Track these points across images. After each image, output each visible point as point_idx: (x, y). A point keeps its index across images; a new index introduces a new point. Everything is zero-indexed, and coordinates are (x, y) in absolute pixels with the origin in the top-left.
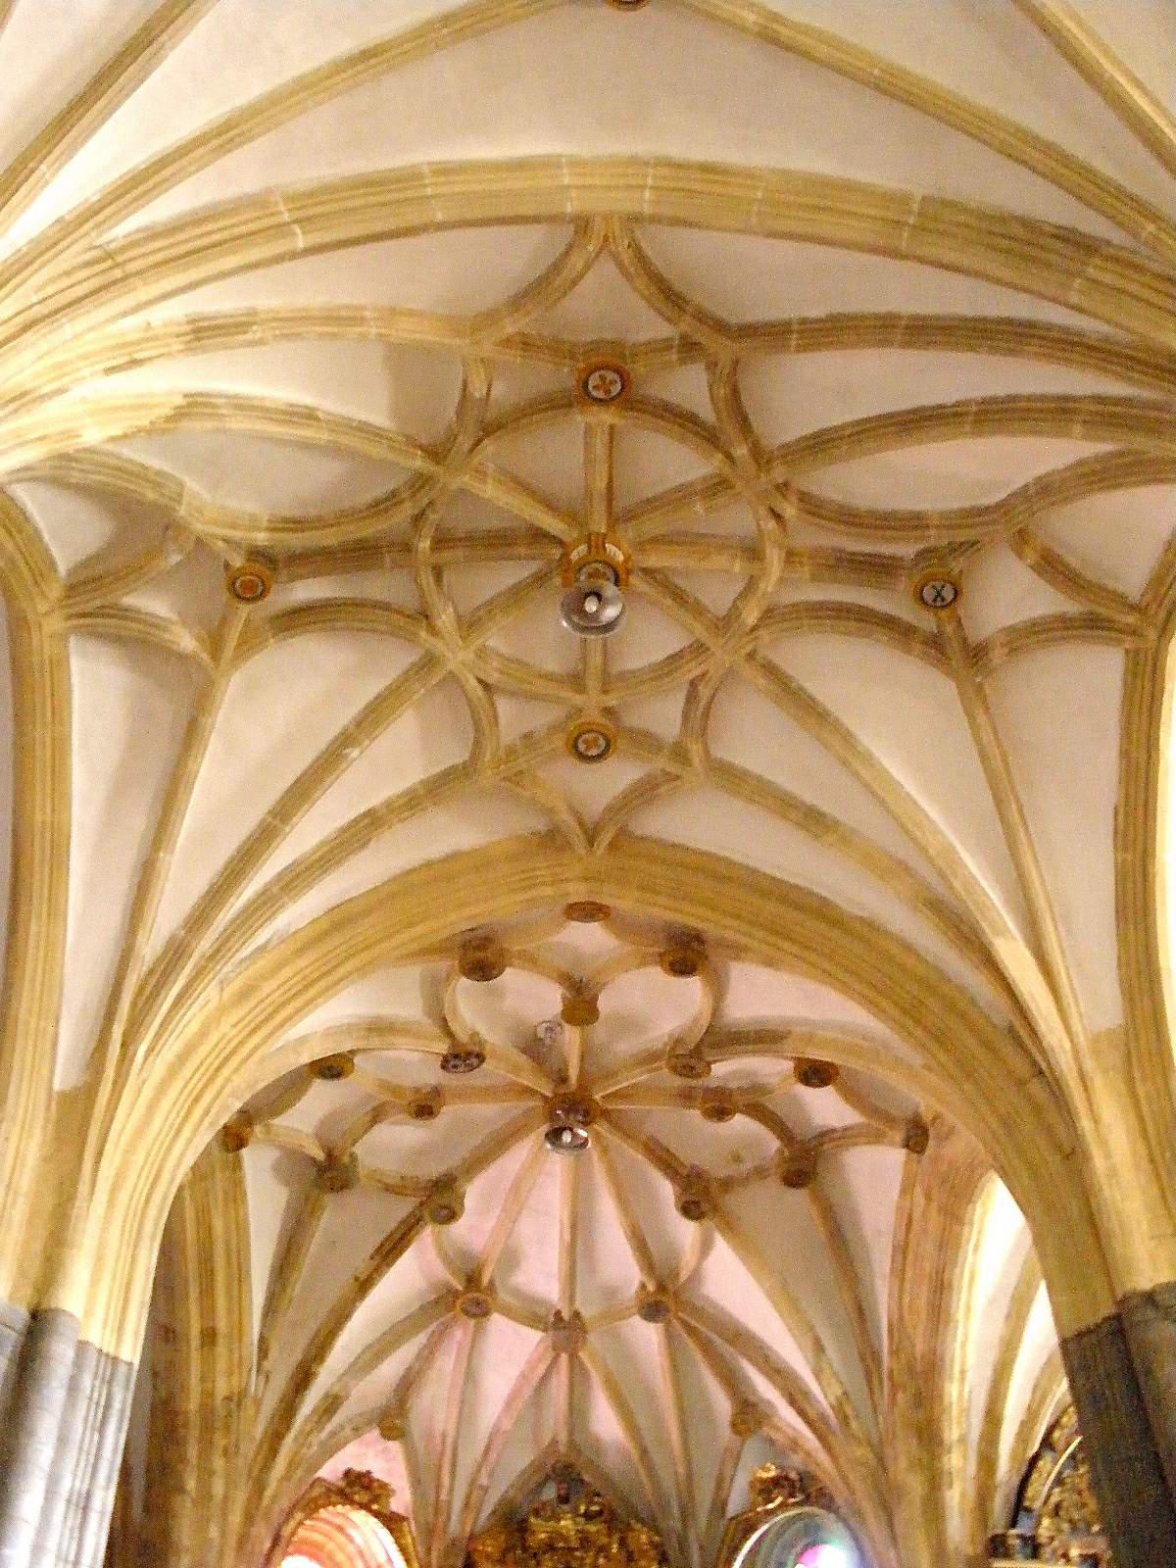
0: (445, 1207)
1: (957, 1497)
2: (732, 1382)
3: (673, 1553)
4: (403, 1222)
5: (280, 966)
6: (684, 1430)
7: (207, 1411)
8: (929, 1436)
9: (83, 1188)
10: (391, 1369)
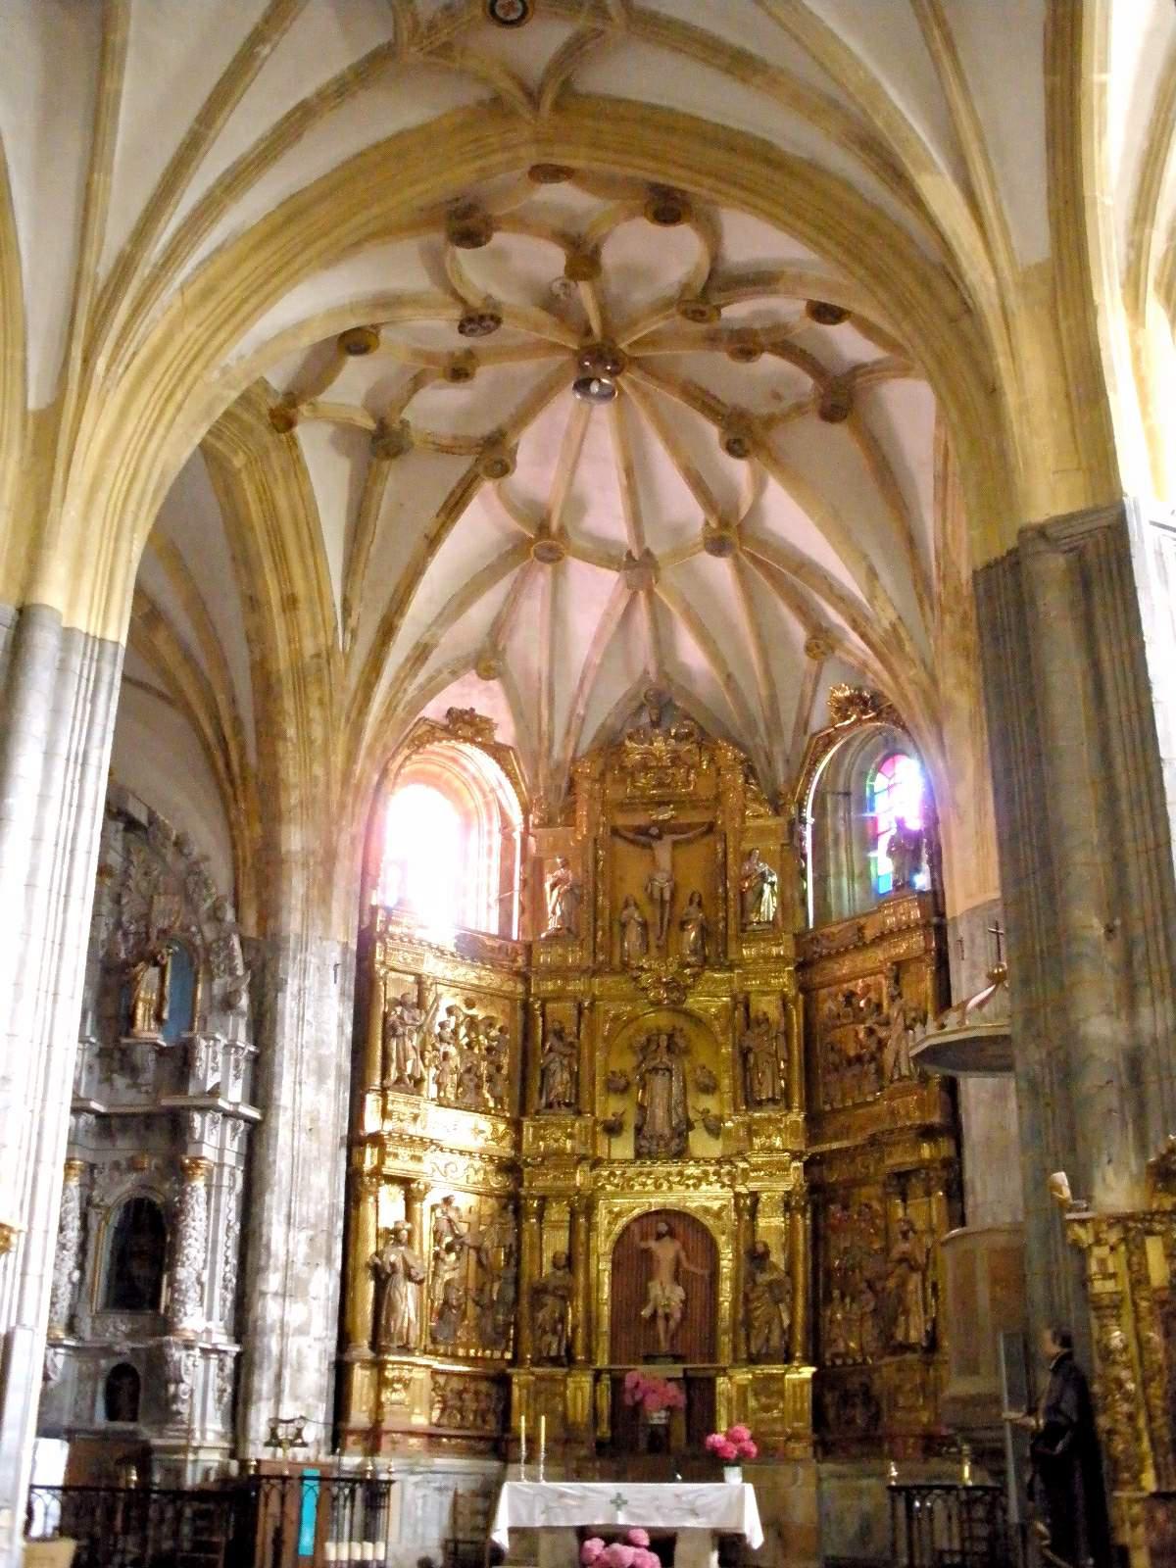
2: (804, 610)
5: (235, 267)
6: (764, 651)
9: (56, 495)
10: (480, 614)
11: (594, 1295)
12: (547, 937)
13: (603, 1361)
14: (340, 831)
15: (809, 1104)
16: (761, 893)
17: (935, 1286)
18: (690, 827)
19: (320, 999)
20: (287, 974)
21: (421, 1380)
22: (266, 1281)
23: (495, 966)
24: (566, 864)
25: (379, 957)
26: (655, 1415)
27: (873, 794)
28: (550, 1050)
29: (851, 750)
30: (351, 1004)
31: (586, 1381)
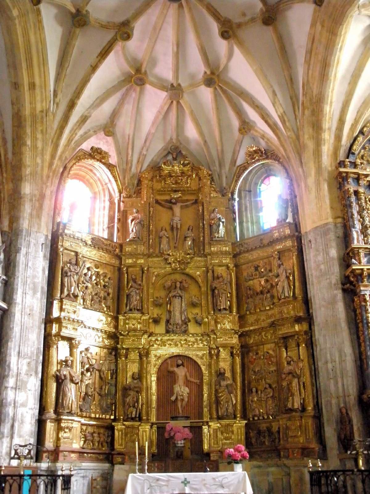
0: (126, 33)
1: (327, 149)
3: (216, 178)
4: (109, 42)
7: (34, 116)
8: (317, 127)
10: (108, 107)
11: (149, 392)
12: (130, 241)
13: (154, 419)
14: (47, 187)
15: (238, 311)
16: (219, 225)
17: (304, 383)
18: (187, 201)
19: (35, 258)
20: (21, 245)
21: (76, 428)
22: (8, 382)
23: (107, 251)
24: (137, 212)
25: (60, 244)
26: (179, 442)
27: (260, 192)
28: (131, 287)
29: (252, 174)
30: (48, 262)
31: (148, 427)
